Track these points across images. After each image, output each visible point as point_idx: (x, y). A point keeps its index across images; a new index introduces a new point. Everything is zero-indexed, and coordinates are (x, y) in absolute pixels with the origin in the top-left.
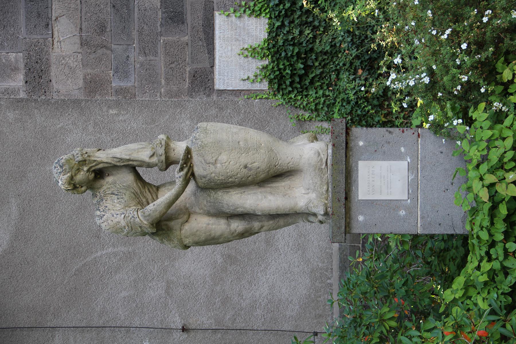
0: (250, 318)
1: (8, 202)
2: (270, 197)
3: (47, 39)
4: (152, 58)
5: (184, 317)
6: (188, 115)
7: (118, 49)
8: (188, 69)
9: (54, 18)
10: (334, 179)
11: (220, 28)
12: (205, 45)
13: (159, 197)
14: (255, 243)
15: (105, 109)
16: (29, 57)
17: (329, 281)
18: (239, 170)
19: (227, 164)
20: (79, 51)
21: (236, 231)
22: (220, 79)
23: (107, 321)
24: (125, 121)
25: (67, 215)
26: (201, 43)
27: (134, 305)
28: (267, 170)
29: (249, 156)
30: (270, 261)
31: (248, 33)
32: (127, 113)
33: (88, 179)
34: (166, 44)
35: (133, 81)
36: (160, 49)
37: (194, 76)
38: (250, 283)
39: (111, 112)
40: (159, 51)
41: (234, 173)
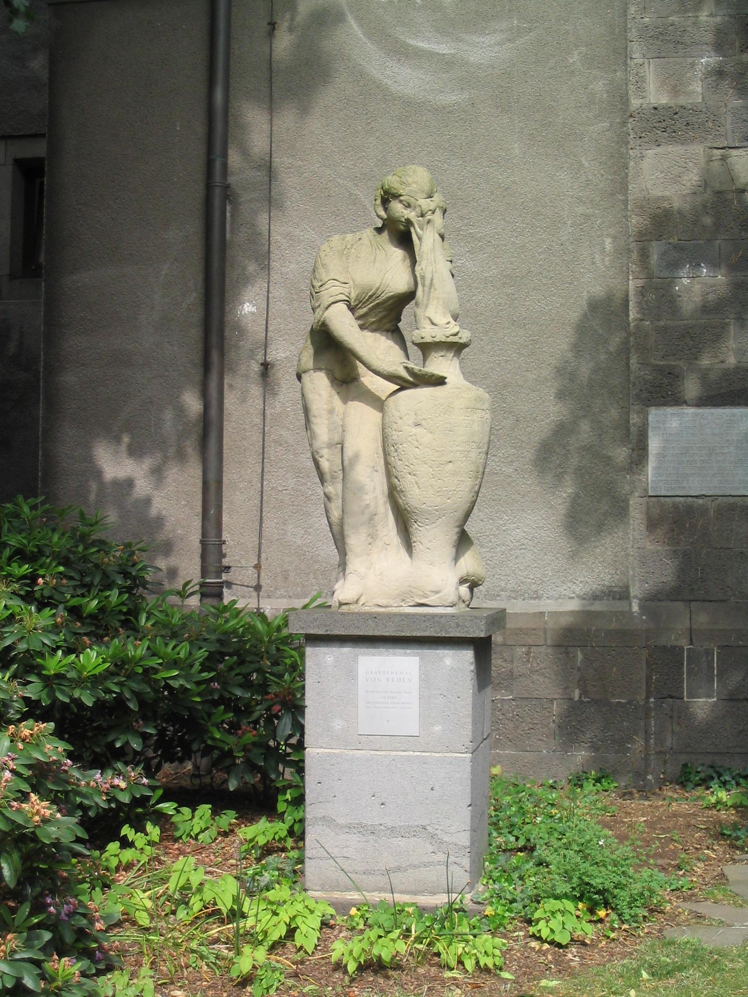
1: (462, 89)
5: (284, 365)
10: (391, 616)
12: (722, 391)
21: (321, 457)
23: (280, 247)
24: (593, 263)
25: (443, 177)
32: (606, 267)
35: (662, 275)
39: (608, 241)
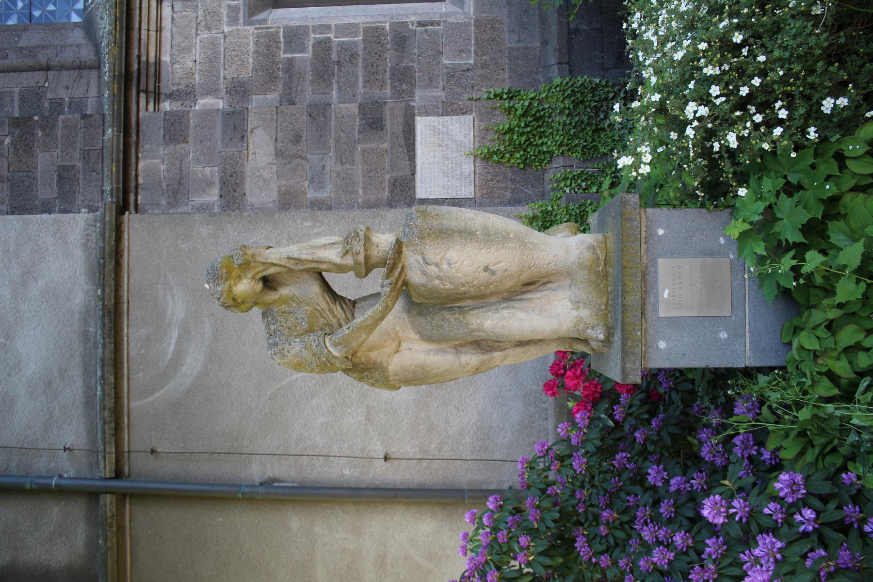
0: (458, 447)
2: (521, 315)
3: (242, 151)
4: (349, 167)
6: (388, 226)
7: (314, 158)
8: (387, 177)
9: (249, 130)
11: (421, 133)
12: (405, 151)
13: (356, 315)
15: (299, 221)
16: (224, 170)
17: (544, 406)
19: (458, 265)
20: (274, 162)
22: (422, 187)
26: (401, 150)
27: (333, 432)
28: (518, 274)
30: (479, 385)
31: (452, 139)
34: (364, 151)
36: (358, 158)
37: (394, 184)
38: (457, 408)
39: (306, 224)
40: (357, 160)
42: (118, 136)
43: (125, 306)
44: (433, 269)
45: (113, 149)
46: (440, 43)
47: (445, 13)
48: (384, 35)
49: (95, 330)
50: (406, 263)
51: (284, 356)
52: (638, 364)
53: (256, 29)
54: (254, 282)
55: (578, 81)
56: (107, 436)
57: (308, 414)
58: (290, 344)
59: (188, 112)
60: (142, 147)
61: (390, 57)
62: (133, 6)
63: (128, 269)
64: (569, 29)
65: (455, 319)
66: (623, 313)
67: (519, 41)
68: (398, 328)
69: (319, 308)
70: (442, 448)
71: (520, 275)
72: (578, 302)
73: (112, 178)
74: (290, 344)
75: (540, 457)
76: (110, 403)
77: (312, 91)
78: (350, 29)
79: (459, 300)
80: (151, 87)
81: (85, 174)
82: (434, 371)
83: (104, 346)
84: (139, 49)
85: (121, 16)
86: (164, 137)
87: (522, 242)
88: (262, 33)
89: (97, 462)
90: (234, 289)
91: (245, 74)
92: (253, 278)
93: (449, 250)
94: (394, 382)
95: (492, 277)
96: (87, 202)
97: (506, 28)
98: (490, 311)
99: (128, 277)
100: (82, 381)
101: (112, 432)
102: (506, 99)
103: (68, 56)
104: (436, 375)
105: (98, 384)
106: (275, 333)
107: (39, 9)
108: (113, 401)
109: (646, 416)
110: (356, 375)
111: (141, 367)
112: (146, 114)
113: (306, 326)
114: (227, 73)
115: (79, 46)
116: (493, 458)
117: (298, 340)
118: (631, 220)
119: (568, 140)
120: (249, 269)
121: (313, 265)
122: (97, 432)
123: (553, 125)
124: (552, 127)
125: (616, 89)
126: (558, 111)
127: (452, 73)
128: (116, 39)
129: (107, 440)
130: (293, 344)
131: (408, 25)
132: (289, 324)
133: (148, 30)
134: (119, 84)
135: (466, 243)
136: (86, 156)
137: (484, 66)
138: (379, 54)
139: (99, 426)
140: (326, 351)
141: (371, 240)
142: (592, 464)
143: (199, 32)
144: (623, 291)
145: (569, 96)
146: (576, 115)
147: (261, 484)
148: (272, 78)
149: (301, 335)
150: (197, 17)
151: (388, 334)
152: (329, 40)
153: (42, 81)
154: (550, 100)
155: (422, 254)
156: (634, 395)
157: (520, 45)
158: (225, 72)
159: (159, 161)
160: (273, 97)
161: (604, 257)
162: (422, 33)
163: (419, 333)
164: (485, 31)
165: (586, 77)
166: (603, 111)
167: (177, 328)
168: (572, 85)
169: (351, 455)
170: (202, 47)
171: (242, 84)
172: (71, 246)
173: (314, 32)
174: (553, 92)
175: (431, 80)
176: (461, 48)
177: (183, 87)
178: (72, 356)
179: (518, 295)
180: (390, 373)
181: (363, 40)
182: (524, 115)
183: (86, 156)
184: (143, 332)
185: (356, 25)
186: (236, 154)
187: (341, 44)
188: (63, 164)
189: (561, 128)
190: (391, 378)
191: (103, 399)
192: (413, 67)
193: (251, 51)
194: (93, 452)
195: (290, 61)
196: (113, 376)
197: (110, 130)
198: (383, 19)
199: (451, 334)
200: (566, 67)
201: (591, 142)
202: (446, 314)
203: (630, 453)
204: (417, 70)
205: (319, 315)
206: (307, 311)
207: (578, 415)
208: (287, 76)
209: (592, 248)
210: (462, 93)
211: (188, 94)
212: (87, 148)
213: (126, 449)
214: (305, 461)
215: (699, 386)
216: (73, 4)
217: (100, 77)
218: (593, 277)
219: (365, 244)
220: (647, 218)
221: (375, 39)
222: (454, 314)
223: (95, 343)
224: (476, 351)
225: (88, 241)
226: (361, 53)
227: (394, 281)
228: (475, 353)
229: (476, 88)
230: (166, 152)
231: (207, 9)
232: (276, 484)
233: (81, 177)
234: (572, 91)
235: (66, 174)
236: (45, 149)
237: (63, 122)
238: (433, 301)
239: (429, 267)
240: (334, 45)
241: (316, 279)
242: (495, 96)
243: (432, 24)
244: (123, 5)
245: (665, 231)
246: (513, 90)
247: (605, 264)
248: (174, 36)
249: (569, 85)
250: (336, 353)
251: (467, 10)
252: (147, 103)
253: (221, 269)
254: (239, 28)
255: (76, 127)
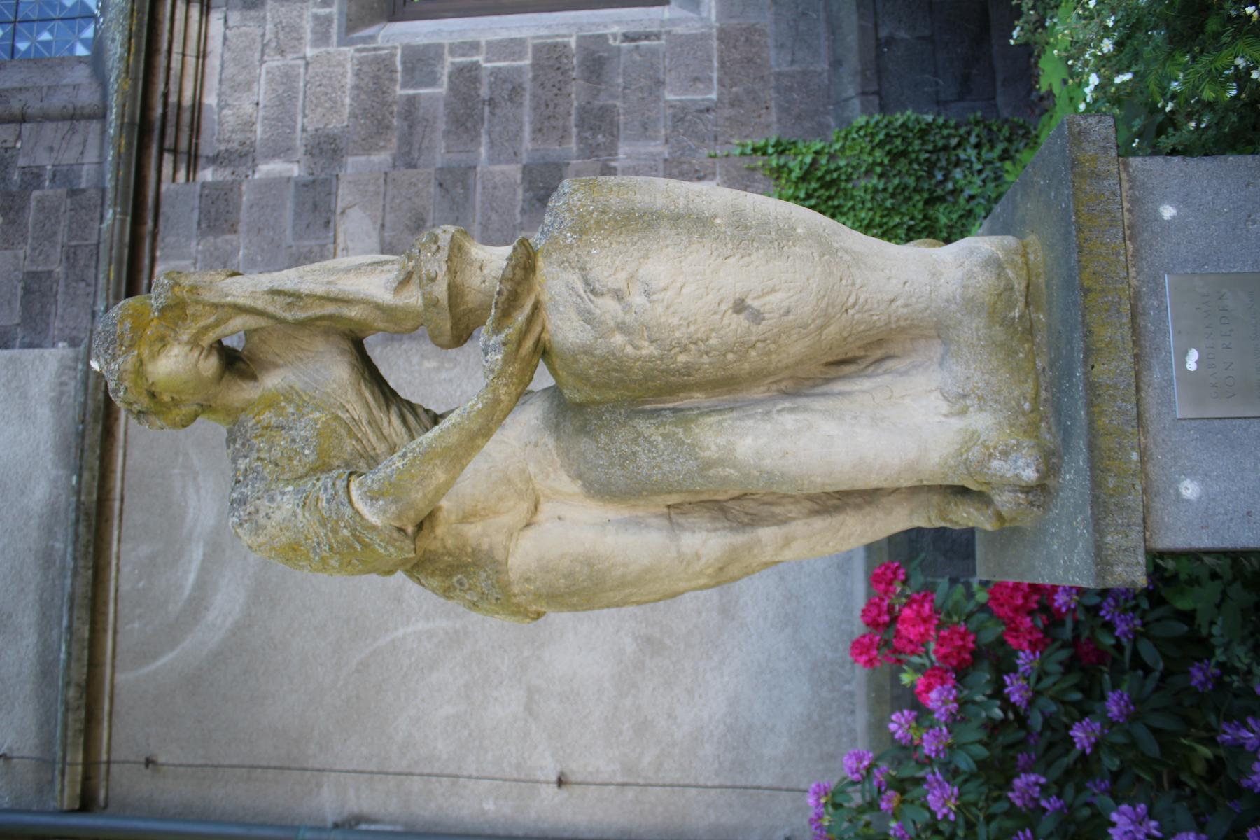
2: (828, 427)
3: (325, 245)
9: (339, 211)
14: (700, 613)
15: (415, 360)
17: (847, 688)
18: (718, 317)
19: (669, 293)
24: (451, 380)
28: (819, 322)
29: (752, 267)
32: (455, 367)
33: (198, 373)
41: (696, 331)
42: (123, 222)
43: (117, 504)
44: (608, 308)
45: (112, 242)
46: (661, 67)
47: (670, 20)
48: (567, 57)
49: (62, 545)
50: (544, 298)
51: (258, 529)
52: (1135, 536)
53: (358, 50)
54: (196, 354)
55: (897, 120)
56: (70, 734)
57: (423, 700)
58: (272, 499)
59: (240, 183)
60: (163, 240)
61: (576, 93)
62: (160, 17)
63: (126, 441)
64: (877, 39)
65: (665, 436)
66: (1090, 405)
67: (793, 62)
68: (532, 469)
69: (345, 416)
70: (661, 764)
71: (822, 328)
72: (965, 396)
73: (108, 289)
74: (272, 499)
75: (854, 783)
76: (79, 673)
77: (448, 147)
78: (512, 47)
79: (673, 390)
80: (184, 145)
81: (67, 286)
82: (619, 572)
83: (75, 572)
84: (167, 84)
85: (139, 30)
86: (199, 224)
87: (827, 249)
88: (366, 57)
89: (52, 782)
90: (150, 368)
91: (337, 123)
92: (194, 343)
93: (646, 257)
94: (522, 599)
95: (754, 328)
96: (67, 331)
97: (770, 42)
98: (749, 416)
99: (125, 455)
100: (36, 636)
101: (80, 726)
102: (771, 155)
103: (57, 102)
104: (623, 583)
105: (63, 640)
106: (245, 476)
107: (26, 39)
108: (85, 670)
109: (1077, 696)
110: (435, 582)
111: (138, 611)
112: (173, 186)
113: (313, 458)
114: (307, 122)
115: (76, 87)
116: (755, 784)
117: (290, 488)
118: (1096, 176)
119: (882, 217)
120: (184, 320)
121: (330, 309)
122: (56, 725)
123: (855, 193)
124: (853, 198)
125: (962, 131)
126: (863, 169)
127: (680, 116)
128: (128, 67)
129: (69, 741)
130: (279, 498)
131: (607, 40)
132: (276, 453)
133: (184, 55)
134: (129, 137)
135: (690, 243)
136: (71, 256)
137: (735, 102)
138: (558, 85)
139: (60, 715)
140: (348, 511)
141: (467, 253)
142: (971, 797)
143: (265, 58)
144: (1088, 351)
145: (881, 144)
146: (895, 176)
147: (336, 826)
148: (382, 128)
149: (301, 478)
150: (263, 35)
151: (508, 481)
152: (475, 66)
153: (11, 139)
154: (848, 153)
155: (582, 269)
156: (1045, 654)
157: (796, 68)
158: (305, 120)
159: (188, 262)
160: (382, 158)
161: (1024, 285)
162: (630, 51)
163: (580, 476)
164: (735, 47)
165: (909, 112)
166: (941, 169)
167: (201, 544)
168: (887, 126)
169: (497, 776)
170: (270, 82)
171: (332, 139)
172: (33, 403)
173: (452, 53)
174: (854, 139)
175: (645, 126)
176: (695, 75)
177: (235, 145)
178: (22, 590)
179: (816, 386)
180: (513, 576)
181: (533, 65)
182: (804, 178)
183: (72, 256)
184: (144, 550)
185: (521, 42)
186: (316, 249)
187: (495, 72)
188: (34, 269)
189: (869, 197)
190: (516, 590)
191: (68, 666)
192: (615, 106)
193: (349, 86)
194: (44, 763)
195: (412, 100)
196: (87, 627)
197: (111, 211)
198: (564, 31)
199: (656, 475)
200: (875, 100)
201: (922, 221)
202: (644, 426)
203: (1044, 775)
204: (621, 111)
205: (343, 432)
206: (316, 421)
207: (934, 695)
208: (405, 124)
209: (993, 264)
210: (698, 148)
211: (243, 156)
212: (74, 243)
213: (104, 757)
214: (416, 784)
215: (1212, 623)
216: (80, 31)
217: (104, 131)
218: (999, 333)
219: (450, 259)
220: (1132, 180)
221: (552, 62)
222: (663, 424)
223: (63, 568)
224: (718, 525)
225: (62, 393)
226: (528, 85)
227: (514, 338)
228: (716, 530)
229: (721, 139)
230: (200, 248)
231: (281, 22)
232: (363, 827)
233: (61, 289)
234: (887, 135)
235: (36, 286)
236: (6, 246)
237: (39, 201)
238: (612, 395)
239: (599, 301)
240: (484, 74)
241: (343, 352)
242: (755, 150)
243: (647, 37)
244: (143, 14)
245: (1179, 210)
246: (784, 140)
247: (1027, 304)
248: (225, 65)
249: (882, 125)
250: (372, 515)
251: (704, 14)
252: (175, 170)
253: (122, 321)
254: (331, 49)
255: (57, 209)
